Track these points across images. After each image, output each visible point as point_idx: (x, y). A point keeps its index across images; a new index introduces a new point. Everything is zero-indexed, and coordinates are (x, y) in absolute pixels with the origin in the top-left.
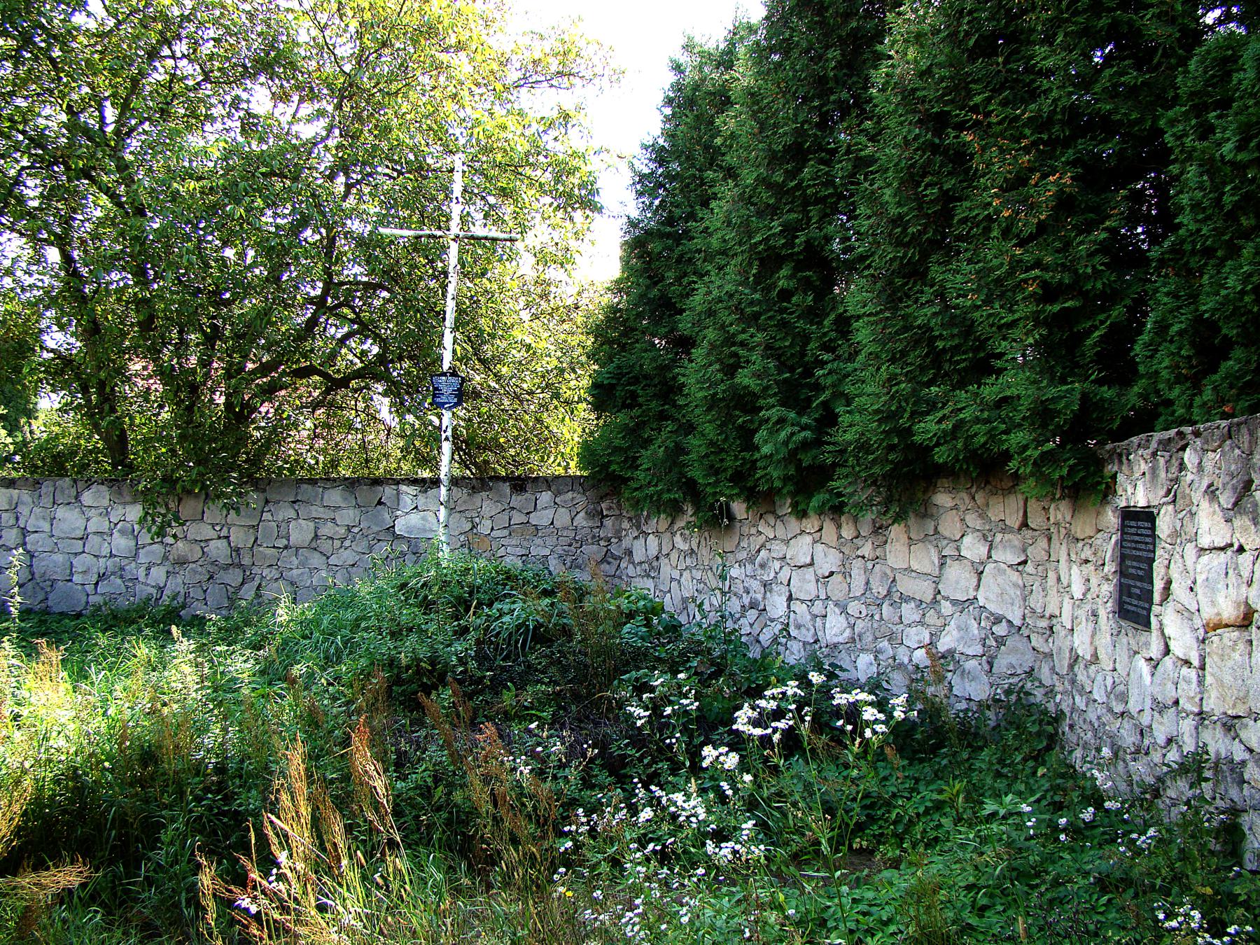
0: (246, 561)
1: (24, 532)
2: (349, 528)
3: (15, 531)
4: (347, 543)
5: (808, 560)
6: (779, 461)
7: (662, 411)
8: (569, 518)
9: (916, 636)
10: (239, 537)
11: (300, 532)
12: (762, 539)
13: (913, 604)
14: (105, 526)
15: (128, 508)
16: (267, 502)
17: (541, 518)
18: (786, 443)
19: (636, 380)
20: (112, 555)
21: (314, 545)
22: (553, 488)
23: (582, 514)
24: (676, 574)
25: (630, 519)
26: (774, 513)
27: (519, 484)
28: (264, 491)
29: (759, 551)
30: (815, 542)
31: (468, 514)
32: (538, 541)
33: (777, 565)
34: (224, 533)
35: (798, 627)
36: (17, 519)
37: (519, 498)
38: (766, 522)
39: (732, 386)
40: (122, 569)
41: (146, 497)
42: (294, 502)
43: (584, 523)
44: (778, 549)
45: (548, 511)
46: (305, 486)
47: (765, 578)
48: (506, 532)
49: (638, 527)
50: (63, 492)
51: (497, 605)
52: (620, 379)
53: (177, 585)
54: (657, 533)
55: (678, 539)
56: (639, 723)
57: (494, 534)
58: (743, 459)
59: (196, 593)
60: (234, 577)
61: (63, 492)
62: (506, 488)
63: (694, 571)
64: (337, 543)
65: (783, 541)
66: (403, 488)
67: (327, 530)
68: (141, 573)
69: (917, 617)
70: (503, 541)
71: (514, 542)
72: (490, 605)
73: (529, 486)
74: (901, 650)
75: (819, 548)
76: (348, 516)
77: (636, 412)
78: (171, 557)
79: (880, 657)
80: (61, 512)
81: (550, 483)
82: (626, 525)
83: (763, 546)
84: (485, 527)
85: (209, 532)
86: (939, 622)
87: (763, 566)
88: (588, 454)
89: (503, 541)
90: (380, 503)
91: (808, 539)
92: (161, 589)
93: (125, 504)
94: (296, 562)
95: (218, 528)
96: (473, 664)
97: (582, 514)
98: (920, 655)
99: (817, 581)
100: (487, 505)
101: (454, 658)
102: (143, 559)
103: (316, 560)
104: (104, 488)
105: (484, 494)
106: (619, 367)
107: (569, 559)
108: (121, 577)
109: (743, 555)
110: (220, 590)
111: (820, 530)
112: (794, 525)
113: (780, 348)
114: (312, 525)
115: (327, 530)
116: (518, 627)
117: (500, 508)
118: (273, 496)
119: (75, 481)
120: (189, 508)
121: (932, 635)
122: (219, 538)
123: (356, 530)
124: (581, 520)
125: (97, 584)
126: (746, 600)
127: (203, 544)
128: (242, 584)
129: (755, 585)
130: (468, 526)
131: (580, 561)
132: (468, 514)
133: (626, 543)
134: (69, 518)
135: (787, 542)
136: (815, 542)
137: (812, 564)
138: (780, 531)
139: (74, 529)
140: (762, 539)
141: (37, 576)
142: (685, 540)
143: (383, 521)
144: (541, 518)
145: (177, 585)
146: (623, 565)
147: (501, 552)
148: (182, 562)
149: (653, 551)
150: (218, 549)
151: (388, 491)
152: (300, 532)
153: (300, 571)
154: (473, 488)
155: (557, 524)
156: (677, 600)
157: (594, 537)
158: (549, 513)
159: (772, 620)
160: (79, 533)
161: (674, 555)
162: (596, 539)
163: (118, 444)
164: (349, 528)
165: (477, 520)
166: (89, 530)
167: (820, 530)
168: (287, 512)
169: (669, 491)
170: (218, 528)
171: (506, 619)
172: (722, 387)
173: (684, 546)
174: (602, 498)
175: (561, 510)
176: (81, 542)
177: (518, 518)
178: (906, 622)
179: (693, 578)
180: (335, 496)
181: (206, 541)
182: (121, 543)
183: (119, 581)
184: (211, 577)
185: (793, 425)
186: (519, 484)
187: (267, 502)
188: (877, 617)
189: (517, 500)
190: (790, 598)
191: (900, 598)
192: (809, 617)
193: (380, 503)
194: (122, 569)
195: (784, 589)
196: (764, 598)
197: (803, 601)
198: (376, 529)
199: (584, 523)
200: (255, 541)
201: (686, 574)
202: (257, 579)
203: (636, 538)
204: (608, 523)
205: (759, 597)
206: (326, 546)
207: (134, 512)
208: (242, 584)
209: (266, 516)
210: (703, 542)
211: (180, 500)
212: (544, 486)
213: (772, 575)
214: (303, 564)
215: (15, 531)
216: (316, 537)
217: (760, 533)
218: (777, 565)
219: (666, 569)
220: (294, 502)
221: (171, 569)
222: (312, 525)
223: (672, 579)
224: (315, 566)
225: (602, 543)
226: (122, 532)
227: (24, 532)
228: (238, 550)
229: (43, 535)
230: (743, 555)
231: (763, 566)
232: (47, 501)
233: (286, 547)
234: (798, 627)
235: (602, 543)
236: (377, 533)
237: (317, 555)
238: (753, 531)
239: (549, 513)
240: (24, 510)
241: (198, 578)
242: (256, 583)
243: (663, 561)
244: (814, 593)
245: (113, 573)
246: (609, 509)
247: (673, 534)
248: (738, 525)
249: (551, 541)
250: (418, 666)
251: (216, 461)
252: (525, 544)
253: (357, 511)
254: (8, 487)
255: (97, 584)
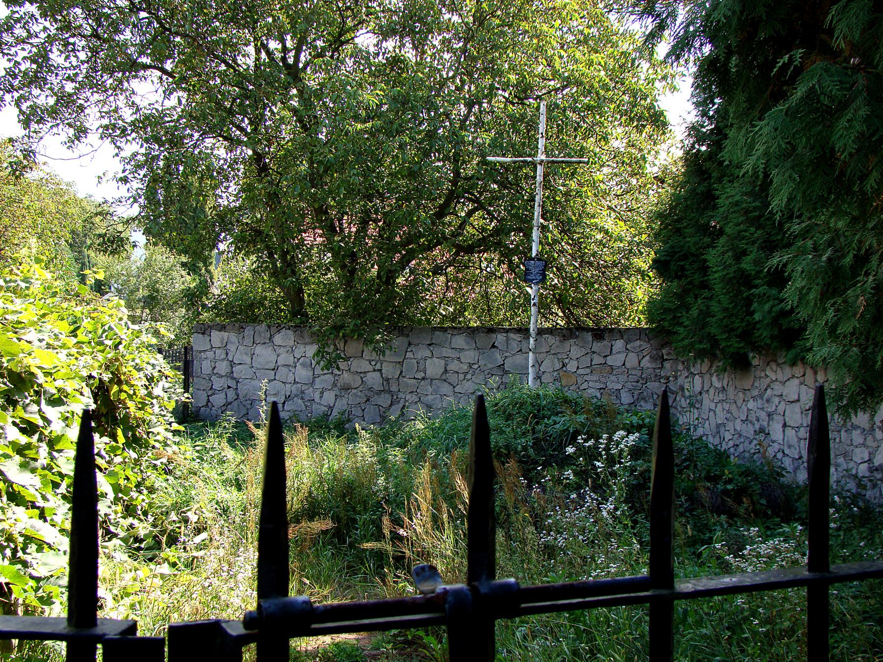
0: (394, 388)
1: (232, 364)
2: (470, 365)
3: (225, 363)
4: (469, 376)
5: (796, 397)
6: (768, 325)
7: (703, 281)
8: (637, 361)
9: (860, 454)
10: (389, 370)
11: (434, 367)
12: (768, 380)
13: (859, 431)
14: (291, 360)
15: (308, 347)
16: (410, 344)
17: (615, 360)
18: (770, 311)
19: (685, 257)
20: (295, 382)
21: (444, 377)
22: (625, 337)
23: (647, 358)
24: (713, 406)
25: (683, 363)
26: (775, 361)
27: (599, 333)
28: (408, 336)
29: (766, 390)
30: (801, 384)
31: (560, 356)
32: (613, 378)
33: (776, 400)
34: (378, 367)
35: (790, 447)
36: (227, 354)
37: (599, 344)
38: (771, 368)
39: (739, 269)
40: (303, 392)
41: (320, 338)
42: (429, 345)
43: (649, 365)
44: (778, 388)
45: (620, 355)
46: (437, 333)
47: (769, 410)
48: (588, 371)
49: (688, 370)
50: (260, 335)
51: (553, 418)
52: (673, 256)
53: (343, 405)
54: (701, 374)
55: (714, 379)
56: (599, 470)
57: (579, 371)
58: (748, 321)
59: (357, 412)
60: (384, 400)
61: (260, 335)
62: (589, 337)
63: (724, 404)
64: (461, 376)
65: (781, 382)
66: (512, 335)
67: (454, 366)
68: (317, 396)
69: (861, 441)
70: (586, 378)
71: (594, 379)
72: (549, 419)
73: (606, 335)
74: (851, 464)
75: (803, 387)
76: (470, 356)
77: (684, 282)
78: (339, 385)
79: (839, 469)
80: (259, 350)
81: (622, 333)
82: (680, 367)
83: (768, 386)
84: (572, 366)
85: (364, 367)
86: (875, 444)
87: (768, 401)
88: (654, 309)
89: (586, 378)
90: (493, 346)
91: (796, 382)
92: (331, 408)
93: (305, 344)
94: (430, 390)
95: (373, 363)
96: (531, 451)
97: (647, 358)
98: (863, 469)
99: (802, 413)
100: (574, 350)
101: (520, 447)
102: (318, 384)
103: (445, 388)
104: (290, 332)
105: (572, 341)
106: (672, 247)
107: (637, 392)
108: (302, 398)
109: (755, 393)
110: (374, 409)
111: (804, 375)
112: (788, 371)
113: (774, 241)
114: (443, 362)
115: (454, 366)
116: (564, 431)
117: (584, 351)
118: (414, 340)
119: (269, 327)
120: (353, 347)
121: (870, 454)
122: (374, 370)
123: (476, 366)
124: (646, 362)
125: (284, 403)
126: (757, 427)
127: (362, 375)
128: (391, 405)
129: (763, 415)
130: (558, 366)
131: (645, 394)
132: (560, 356)
133: (680, 381)
134: (265, 355)
135: (784, 383)
136: (801, 384)
137: (798, 400)
138: (780, 376)
139: (268, 363)
140: (768, 380)
141: (241, 396)
142: (719, 379)
143: (496, 360)
144: (615, 360)
145: (343, 405)
146: (678, 399)
147: (585, 386)
148: (347, 388)
149: (698, 388)
150: (374, 379)
151: (500, 338)
152: (434, 367)
153: (433, 397)
154: (564, 336)
155: (628, 365)
156: (713, 426)
157: (656, 376)
158: (622, 357)
159: (773, 442)
160: (272, 366)
161: (712, 391)
162: (658, 378)
163: (295, 295)
164: (470, 365)
165: (567, 361)
166: (279, 363)
167: (804, 375)
168: (423, 352)
169: (700, 342)
170: (373, 363)
171: (557, 426)
172: (733, 269)
173: (718, 384)
174: (663, 346)
175: (631, 354)
176: (273, 372)
177: (598, 360)
178: (855, 444)
179: (724, 409)
180: (460, 341)
181: (365, 373)
182: (303, 373)
183: (300, 401)
184: (368, 400)
185: (775, 299)
186: (599, 333)
187: (410, 344)
188: (837, 440)
189: (597, 346)
190: (785, 425)
191: (852, 426)
192: (796, 440)
193: (493, 346)
194: (303, 392)
195: (781, 418)
196: (768, 425)
197: (793, 428)
198: (490, 366)
199: (649, 365)
200: (401, 373)
201: (719, 405)
202: (402, 401)
203: (687, 377)
204: (667, 365)
205: (765, 424)
206: (453, 378)
207: (312, 350)
208: (391, 405)
209: (409, 355)
210: (731, 382)
211: (346, 342)
212: (618, 336)
213: (774, 407)
214: (436, 392)
215: (225, 363)
216: (446, 371)
217: (767, 376)
218: (776, 400)
219: (707, 403)
220: (429, 345)
221: (338, 393)
222: (443, 362)
223: (710, 410)
224: (444, 385)
225: (663, 381)
226: (304, 365)
227: (232, 364)
228: (388, 380)
229: (246, 366)
230: (755, 393)
231: (768, 401)
232: (248, 341)
233: (423, 379)
234: (790, 447)
235: (663, 381)
236: (492, 369)
237: (446, 385)
238: (763, 374)
239: (622, 357)
240: (232, 348)
241: (358, 400)
242: (401, 406)
243: (705, 395)
244: (800, 422)
245: (296, 396)
246: (668, 354)
247: (711, 375)
248: (753, 369)
249: (623, 378)
250: (498, 450)
251: (374, 314)
252: (603, 380)
253: (477, 353)
254: (220, 331)
255: (284, 403)
